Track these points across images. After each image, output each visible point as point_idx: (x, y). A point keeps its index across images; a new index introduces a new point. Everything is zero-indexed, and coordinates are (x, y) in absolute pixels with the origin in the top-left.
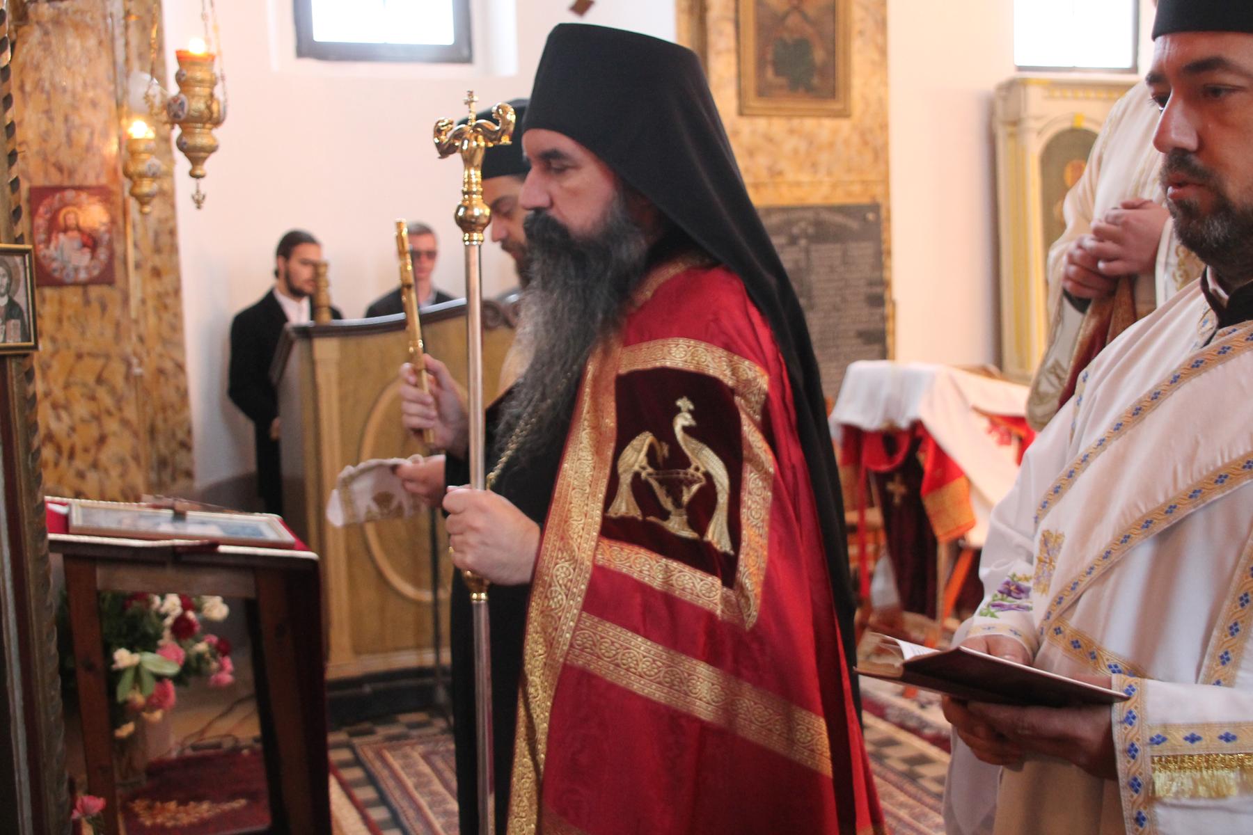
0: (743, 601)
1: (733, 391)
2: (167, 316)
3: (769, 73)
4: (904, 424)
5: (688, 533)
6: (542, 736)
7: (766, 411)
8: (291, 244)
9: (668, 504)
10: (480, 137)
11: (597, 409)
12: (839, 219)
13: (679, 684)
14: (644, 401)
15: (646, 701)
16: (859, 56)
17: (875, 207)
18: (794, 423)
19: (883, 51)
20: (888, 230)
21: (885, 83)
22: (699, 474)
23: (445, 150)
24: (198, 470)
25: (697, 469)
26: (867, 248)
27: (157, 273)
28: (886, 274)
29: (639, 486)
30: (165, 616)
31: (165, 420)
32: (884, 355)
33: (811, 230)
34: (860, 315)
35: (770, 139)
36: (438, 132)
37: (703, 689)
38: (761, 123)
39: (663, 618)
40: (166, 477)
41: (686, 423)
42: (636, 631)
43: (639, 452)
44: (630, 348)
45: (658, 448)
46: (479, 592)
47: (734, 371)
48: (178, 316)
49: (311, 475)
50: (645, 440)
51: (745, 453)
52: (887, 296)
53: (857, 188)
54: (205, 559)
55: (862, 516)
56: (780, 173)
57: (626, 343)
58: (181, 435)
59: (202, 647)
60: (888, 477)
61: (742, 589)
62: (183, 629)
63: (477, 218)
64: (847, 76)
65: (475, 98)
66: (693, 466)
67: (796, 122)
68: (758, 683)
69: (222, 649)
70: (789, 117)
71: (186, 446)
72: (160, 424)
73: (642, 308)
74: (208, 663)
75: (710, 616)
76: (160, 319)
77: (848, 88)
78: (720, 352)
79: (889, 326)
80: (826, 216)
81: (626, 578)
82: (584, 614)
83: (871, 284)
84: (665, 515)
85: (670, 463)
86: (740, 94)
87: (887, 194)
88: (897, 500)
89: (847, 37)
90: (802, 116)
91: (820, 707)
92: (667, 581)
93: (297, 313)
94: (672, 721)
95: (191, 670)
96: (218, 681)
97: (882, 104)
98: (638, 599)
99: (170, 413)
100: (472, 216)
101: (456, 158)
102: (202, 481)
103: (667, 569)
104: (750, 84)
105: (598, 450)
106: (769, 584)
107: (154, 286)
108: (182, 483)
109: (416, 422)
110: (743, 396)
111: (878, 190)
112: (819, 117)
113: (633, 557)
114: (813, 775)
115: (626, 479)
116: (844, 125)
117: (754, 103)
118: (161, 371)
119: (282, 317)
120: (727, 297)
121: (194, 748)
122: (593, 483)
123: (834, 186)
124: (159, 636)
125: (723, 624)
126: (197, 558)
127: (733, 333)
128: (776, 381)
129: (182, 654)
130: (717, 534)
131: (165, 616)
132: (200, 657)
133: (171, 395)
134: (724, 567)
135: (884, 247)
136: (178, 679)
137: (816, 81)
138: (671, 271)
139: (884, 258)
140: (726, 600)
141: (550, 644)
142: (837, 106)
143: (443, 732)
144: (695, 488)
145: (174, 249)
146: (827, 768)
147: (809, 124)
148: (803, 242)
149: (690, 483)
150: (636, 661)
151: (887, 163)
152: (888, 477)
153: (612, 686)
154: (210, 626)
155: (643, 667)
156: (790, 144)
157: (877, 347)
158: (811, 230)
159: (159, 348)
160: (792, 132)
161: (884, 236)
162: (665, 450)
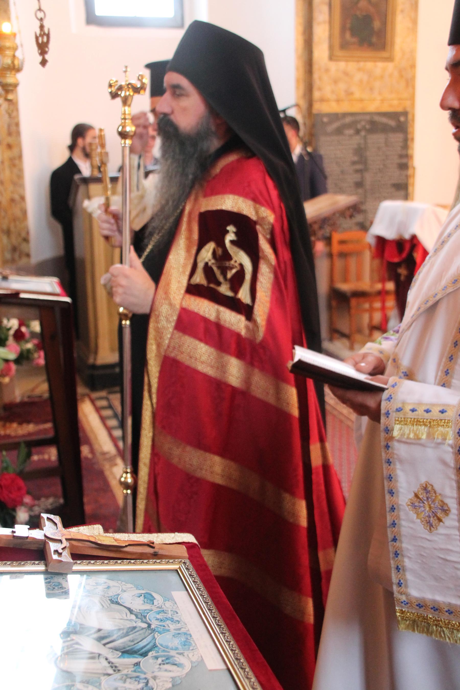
0: (255, 328)
1: (255, 223)
2: (15, 170)
3: (348, 35)
4: (407, 236)
5: (230, 294)
6: (154, 390)
7: (272, 233)
8: (79, 132)
9: (221, 279)
10: (131, 90)
11: (190, 230)
12: (384, 120)
13: (222, 368)
14: (212, 226)
15: (205, 376)
16: (400, 24)
17: (405, 114)
18: (288, 240)
19: (415, 22)
20: (413, 127)
21: (415, 40)
22: (237, 264)
23: (114, 96)
24: (33, 253)
25: (236, 262)
26: (397, 138)
27: (9, 146)
28: (410, 152)
29: (207, 270)
30: (9, 329)
31: (15, 227)
32: (406, 197)
33: (368, 127)
34: (395, 175)
35: (346, 74)
36: (110, 86)
37: (234, 371)
38: (342, 65)
39: (216, 335)
40: (16, 255)
41: (232, 239)
42: (201, 340)
43: (208, 252)
44: (206, 199)
45: (216, 250)
46: (126, 320)
47: (257, 212)
48: (21, 170)
49: (88, 257)
50: (210, 246)
51: (261, 254)
52: (410, 164)
53: (395, 102)
54: (14, 300)
55: (384, 286)
56: (352, 94)
57: (206, 195)
58: (23, 234)
59: (29, 346)
60: (398, 265)
61: (255, 322)
62: (19, 336)
63: (128, 132)
64: (393, 36)
65: (128, 70)
66: (234, 260)
67: (362, 64)
68: (262, 369)
69: (39, 347)
70: (358, 61)
71: (26, 240)
72: (12, 229)
73: (214, 178)
74: (32, 354)
75: (238, 335)
76: (11, 172)
77: (392, 44)
78: (250, 203)
79: (410, 181)
80: (377, 118)
81: (197, 315)
82: (175, 332)
83: (401, 156)
84: (219, 284)
85: (223, 257)
86: (331, 47)
87: (413, 105)
88: (402, 278)
89: (394, 14)
90: (365, 61)
91: (293, 382)
92: (218, 317)
93: (85, 169)
94: (218, 386)
95: (23, 358)
96: (37, 364)
97: (413, 52)
98: (202, 325)
99: (18, 223)
100: (126, 132)
101: (118, 101)
102: (35, 259)
103: (218, 312)
104: (337, 42)
105: (188, 250)
106: (269, 321)
107: (8, 154)
108: (24, 261)
109: (106, 232)
110: (261, 225)
111: (408, 103)
112: (375, 61)
113: (200, 304)
114: (288, 416)
115: (201, 265)
116: (390, 66)
117: (338, 52)
118: (12, 200)
119: (78, 171)
120: (256, 172)
121: (29, 397)
122: (185, 266)
123: (382, 101)
124: (6, 339)
125: (245, 339)
126: (10, 300)
127: (257, 193)
128: (279, 218)
129: (19, 349)
130: (244, 295)
131: (9, 329)
132: (29, 351)
133: (18, 213)
134: (247, 311)
135: (409, 136)
136: (18, 361)
137: (374, 40)
138: (232, 158)
139: (409, 143)
140: (247, 327)
141: (159, 345)
142: (385, 54)
143: (396, 437)
144: (234, 271)
145: (18, 133)
146: (295, 412)
147: (369, 65)
148: (363, 133)
149: (231, 268)
150: (201, 356)
151: (414, 88)
152: (398, 265)
153: (188, 367)
154: (33, 335)
155: (204, 358)
156: (358, 76)
157: (402, 193)
158: (368, 127)
159: (11, 188)
160: (359, 69)
161: (410, 130)
162: (220, 251)
